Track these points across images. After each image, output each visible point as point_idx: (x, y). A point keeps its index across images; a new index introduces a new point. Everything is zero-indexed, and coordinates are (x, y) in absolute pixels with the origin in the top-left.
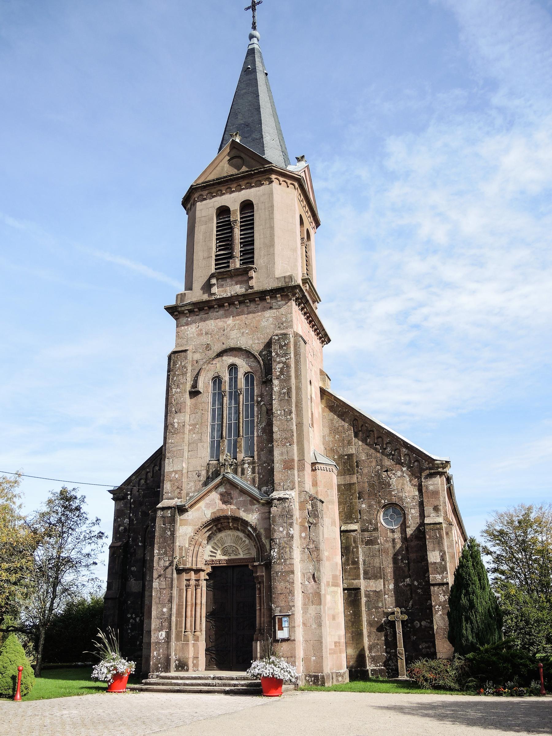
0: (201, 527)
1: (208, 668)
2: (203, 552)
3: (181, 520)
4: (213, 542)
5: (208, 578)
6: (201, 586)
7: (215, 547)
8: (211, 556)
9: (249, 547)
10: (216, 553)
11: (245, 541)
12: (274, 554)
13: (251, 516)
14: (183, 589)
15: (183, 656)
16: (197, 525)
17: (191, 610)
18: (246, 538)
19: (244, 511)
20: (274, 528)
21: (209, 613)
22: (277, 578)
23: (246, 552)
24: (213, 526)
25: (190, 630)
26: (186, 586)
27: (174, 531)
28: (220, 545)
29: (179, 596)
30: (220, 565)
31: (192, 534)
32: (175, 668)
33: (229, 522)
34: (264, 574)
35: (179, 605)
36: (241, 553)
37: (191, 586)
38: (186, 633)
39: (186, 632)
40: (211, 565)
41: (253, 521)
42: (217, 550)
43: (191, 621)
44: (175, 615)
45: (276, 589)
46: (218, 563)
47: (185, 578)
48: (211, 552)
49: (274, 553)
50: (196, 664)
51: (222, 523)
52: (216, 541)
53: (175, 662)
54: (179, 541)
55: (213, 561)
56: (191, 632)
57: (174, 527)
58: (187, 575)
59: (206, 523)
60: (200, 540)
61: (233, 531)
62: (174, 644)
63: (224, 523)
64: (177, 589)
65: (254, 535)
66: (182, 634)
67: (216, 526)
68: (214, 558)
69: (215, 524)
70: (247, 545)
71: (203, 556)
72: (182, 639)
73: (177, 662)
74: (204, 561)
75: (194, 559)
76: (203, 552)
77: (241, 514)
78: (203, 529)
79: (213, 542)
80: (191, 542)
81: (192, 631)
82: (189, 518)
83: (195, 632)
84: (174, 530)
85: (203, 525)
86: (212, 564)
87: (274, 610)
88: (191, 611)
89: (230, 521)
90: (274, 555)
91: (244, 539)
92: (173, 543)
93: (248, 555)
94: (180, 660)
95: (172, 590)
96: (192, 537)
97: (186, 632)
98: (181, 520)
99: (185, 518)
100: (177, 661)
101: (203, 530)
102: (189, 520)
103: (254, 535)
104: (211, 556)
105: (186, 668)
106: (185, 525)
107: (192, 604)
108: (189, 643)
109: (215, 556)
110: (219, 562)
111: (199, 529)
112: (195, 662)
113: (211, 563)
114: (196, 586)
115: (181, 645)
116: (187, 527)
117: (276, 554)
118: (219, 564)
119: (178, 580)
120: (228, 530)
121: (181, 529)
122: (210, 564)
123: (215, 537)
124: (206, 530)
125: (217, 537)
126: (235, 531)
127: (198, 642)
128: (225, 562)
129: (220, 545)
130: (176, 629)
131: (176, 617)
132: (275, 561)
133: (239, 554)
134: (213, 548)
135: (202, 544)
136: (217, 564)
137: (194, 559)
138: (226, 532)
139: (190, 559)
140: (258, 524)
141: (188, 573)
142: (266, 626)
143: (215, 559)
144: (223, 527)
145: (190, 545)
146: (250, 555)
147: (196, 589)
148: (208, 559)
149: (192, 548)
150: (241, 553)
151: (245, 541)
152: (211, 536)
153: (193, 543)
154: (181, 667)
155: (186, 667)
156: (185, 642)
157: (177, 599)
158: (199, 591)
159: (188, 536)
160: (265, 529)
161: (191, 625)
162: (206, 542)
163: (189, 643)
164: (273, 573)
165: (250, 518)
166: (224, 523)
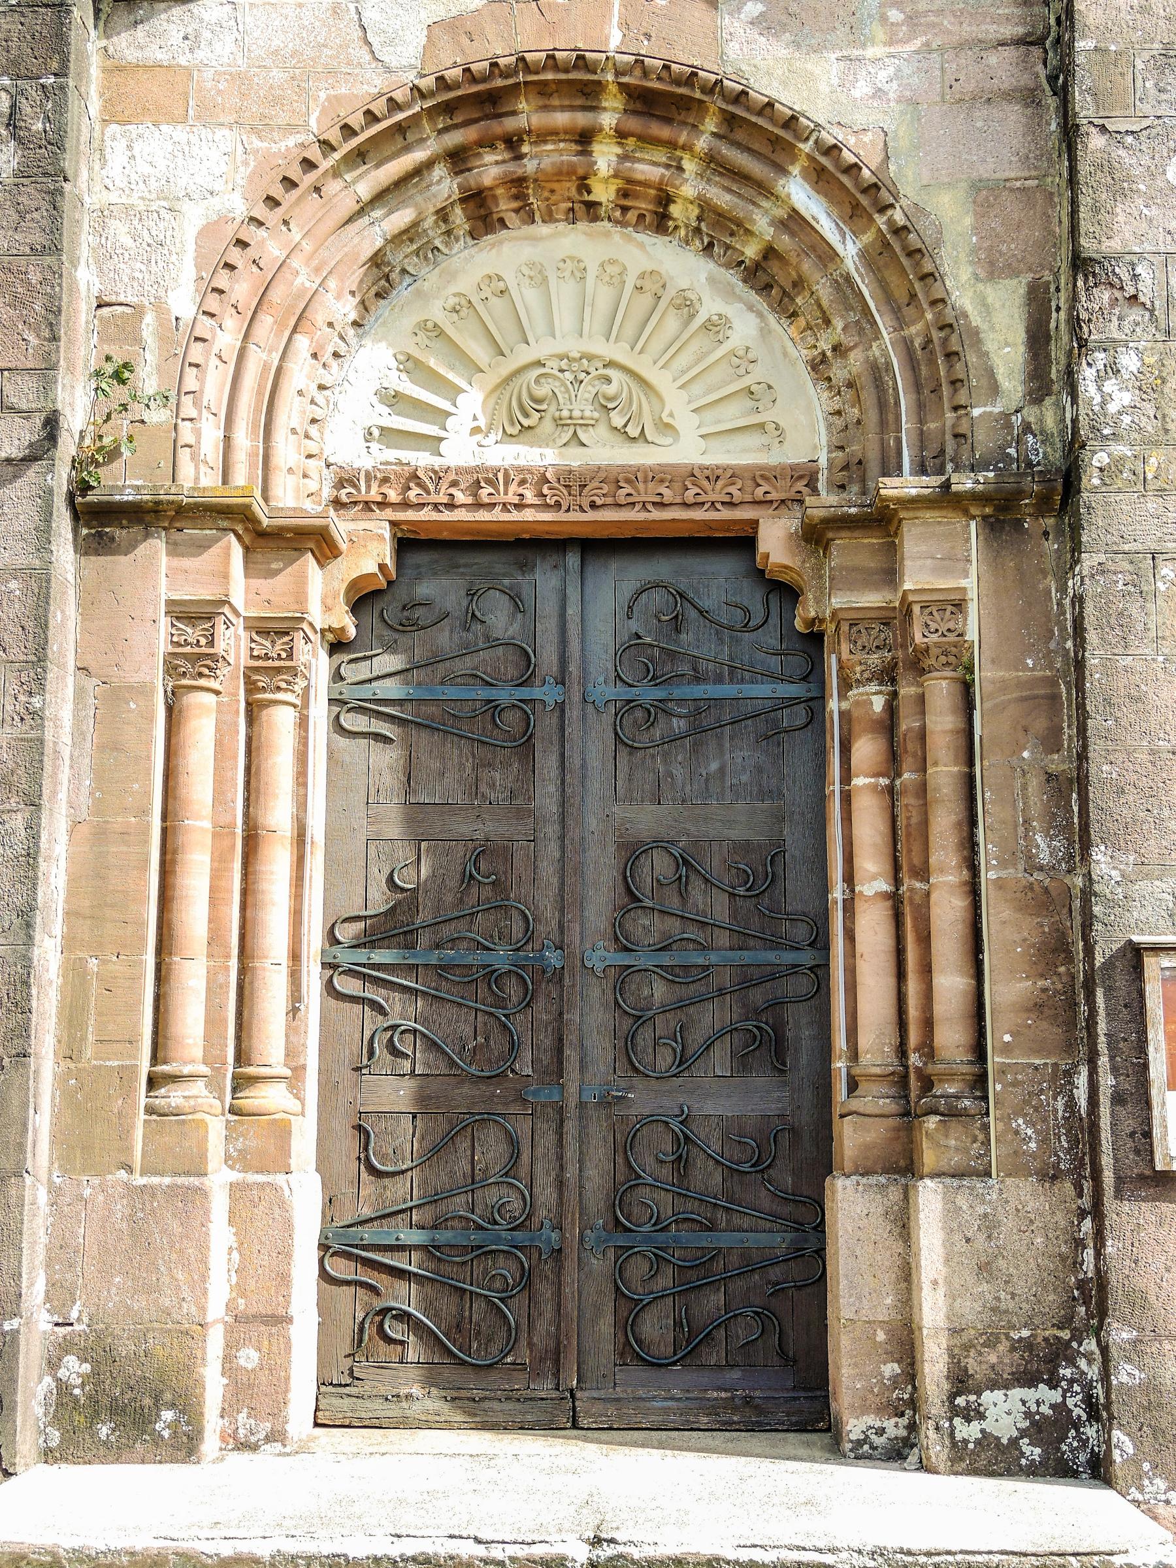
0: (327, 146)
1: (342, 1406)
2: (320, 398)
3: (116, 69)
4: (409, 321)
5: (352, 632)
6: (301, 683)
7: (432, 363)
8: (388, 435)
9: (758, 373)
10: (440, 417)
11: (716, 327)
12: (1106, 399)
13: (836, 68)
14: (144, 691)
15: (139, 1303)
16: (291, 128)
17: (213, 889)
18: (729, 294)
19: (764, 24)
20: (1106, 166)
21: (361, 925)
22: (1135, 612)
23: (734, 414)
24: (429, 164)
25: (204, 1070)
26: (171, 669)
27: (56, 142)
28: (479, 351)
29: (102, 748)
30: (483, 516)
31: (239, 207)
32: (57, 1420)
33: (585, 138)
34: (970, 583)
35: (100, 834)
36: (687, 423)
37: (223, 671)
38: (173, 1097)
39: (174, 1078)
40: (389, 514)
41: (860, 119)
42: (453, 391)
43: (213, 989)
44: (58, 928)
45: (1127, 713)
46: (461, 497)
47: (164, 591)
48: (394, 400)
49: (1109, 386)
50: (263, 1378)
51: (512, 142)
52: (437, 313)
53: (53, 1365)
54: (104, 257)
55: (414, 477)
56: (214, 1084)
57: (61, 108)
58: (187, 563)
59: (371, 117)
60: (304, 280)
61: (607, 234)
62: (43, 1196)
63: (543, 136)
64: (79, 693)
65: (849, 250)
66: (134, 1105)
67: (458, 159)
68: (421, 459)
69: (455, 138)
70: (743, 360)
71: (313, 430)
72: (129, 1149)
73: (74, 1368)
74: (329, 476)
75: (243, 440)
76: (320, 398)
77: (733, 50)
78: (336, 173)
79: (409, 321)
80: (223, 280)
81: (219, 1072)
82: (200, 55)
83: (241, 1083)
84: (61, 132)
85: (348, 131)
86: (405, 505)
87: (1111, 904)
88: (214, 902)
89: (608, 120)
90: (1112, 408)
91: (711, 306)
92: (55, 249)
93: (755, 440)
94: (109, 1350)
95: (39, 685)
96: (229, 232)
97: (174, 1078)
98: (116, 69)
99: (161, 56)
100: (71, 1361)
101: (333, 187)
102: (209, 74)
103: (849, 250)
104: (388, 435)
105: (174, 1426)
106: (160, 114)
107: (221, 832)
108: (207, 1182)
109: (433, 443)
110: (477, 485)
111: (308, 165)
112: (249, 1358)
113: (393, 496)
114: (262, 680)
115: (120, 1208)
116: (180, 133)
117: (1126, 398)
118: (478, 505)
119: (87, 605)
120: (561, 226)
121: (117, 157)
122: (383, 505)
123: (430, 278)
124: (365, 190)
125: (452, 276)
126: (629, 239)
127: (280, 1179)
128: (530, 497)
129: (479, 351)
130: (70, 1053)
131: (69, 944)
132: (1118, 463)
133: (667, 428)
134: (411, 365)
135: (319, 317)
136: (451, 506)
137: (243, 440)
138: (535, 239)
139: (211, 435)
140: (902, 141)
141: (202, 547)
142: (1006, 1049)
143: (437, 462)
144: (518, 184)
145: (213, 303)
146: (768, 447)
147: (253, 711)
148: (366, 463)
149: (227, 339)
150: (687, 423)
151: (716, 327)
152: (396, 258)
153: (242, 289)
154: (116, 1410)
155: (168, 1415)
156: (167, 1180)
157: (76, 777)
158: (281, 720)
159: (194, 217)
160: (976, 186)
161: (213, 1022)
162: (348, 309)
163: (207, 1182)
164: (1101, 569)
165: (824, 88)
166: (543, 136)
